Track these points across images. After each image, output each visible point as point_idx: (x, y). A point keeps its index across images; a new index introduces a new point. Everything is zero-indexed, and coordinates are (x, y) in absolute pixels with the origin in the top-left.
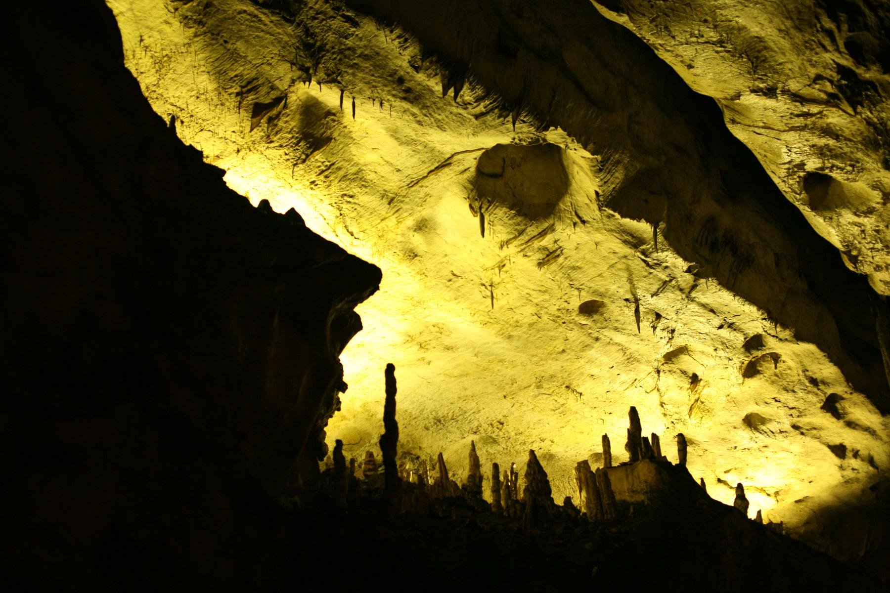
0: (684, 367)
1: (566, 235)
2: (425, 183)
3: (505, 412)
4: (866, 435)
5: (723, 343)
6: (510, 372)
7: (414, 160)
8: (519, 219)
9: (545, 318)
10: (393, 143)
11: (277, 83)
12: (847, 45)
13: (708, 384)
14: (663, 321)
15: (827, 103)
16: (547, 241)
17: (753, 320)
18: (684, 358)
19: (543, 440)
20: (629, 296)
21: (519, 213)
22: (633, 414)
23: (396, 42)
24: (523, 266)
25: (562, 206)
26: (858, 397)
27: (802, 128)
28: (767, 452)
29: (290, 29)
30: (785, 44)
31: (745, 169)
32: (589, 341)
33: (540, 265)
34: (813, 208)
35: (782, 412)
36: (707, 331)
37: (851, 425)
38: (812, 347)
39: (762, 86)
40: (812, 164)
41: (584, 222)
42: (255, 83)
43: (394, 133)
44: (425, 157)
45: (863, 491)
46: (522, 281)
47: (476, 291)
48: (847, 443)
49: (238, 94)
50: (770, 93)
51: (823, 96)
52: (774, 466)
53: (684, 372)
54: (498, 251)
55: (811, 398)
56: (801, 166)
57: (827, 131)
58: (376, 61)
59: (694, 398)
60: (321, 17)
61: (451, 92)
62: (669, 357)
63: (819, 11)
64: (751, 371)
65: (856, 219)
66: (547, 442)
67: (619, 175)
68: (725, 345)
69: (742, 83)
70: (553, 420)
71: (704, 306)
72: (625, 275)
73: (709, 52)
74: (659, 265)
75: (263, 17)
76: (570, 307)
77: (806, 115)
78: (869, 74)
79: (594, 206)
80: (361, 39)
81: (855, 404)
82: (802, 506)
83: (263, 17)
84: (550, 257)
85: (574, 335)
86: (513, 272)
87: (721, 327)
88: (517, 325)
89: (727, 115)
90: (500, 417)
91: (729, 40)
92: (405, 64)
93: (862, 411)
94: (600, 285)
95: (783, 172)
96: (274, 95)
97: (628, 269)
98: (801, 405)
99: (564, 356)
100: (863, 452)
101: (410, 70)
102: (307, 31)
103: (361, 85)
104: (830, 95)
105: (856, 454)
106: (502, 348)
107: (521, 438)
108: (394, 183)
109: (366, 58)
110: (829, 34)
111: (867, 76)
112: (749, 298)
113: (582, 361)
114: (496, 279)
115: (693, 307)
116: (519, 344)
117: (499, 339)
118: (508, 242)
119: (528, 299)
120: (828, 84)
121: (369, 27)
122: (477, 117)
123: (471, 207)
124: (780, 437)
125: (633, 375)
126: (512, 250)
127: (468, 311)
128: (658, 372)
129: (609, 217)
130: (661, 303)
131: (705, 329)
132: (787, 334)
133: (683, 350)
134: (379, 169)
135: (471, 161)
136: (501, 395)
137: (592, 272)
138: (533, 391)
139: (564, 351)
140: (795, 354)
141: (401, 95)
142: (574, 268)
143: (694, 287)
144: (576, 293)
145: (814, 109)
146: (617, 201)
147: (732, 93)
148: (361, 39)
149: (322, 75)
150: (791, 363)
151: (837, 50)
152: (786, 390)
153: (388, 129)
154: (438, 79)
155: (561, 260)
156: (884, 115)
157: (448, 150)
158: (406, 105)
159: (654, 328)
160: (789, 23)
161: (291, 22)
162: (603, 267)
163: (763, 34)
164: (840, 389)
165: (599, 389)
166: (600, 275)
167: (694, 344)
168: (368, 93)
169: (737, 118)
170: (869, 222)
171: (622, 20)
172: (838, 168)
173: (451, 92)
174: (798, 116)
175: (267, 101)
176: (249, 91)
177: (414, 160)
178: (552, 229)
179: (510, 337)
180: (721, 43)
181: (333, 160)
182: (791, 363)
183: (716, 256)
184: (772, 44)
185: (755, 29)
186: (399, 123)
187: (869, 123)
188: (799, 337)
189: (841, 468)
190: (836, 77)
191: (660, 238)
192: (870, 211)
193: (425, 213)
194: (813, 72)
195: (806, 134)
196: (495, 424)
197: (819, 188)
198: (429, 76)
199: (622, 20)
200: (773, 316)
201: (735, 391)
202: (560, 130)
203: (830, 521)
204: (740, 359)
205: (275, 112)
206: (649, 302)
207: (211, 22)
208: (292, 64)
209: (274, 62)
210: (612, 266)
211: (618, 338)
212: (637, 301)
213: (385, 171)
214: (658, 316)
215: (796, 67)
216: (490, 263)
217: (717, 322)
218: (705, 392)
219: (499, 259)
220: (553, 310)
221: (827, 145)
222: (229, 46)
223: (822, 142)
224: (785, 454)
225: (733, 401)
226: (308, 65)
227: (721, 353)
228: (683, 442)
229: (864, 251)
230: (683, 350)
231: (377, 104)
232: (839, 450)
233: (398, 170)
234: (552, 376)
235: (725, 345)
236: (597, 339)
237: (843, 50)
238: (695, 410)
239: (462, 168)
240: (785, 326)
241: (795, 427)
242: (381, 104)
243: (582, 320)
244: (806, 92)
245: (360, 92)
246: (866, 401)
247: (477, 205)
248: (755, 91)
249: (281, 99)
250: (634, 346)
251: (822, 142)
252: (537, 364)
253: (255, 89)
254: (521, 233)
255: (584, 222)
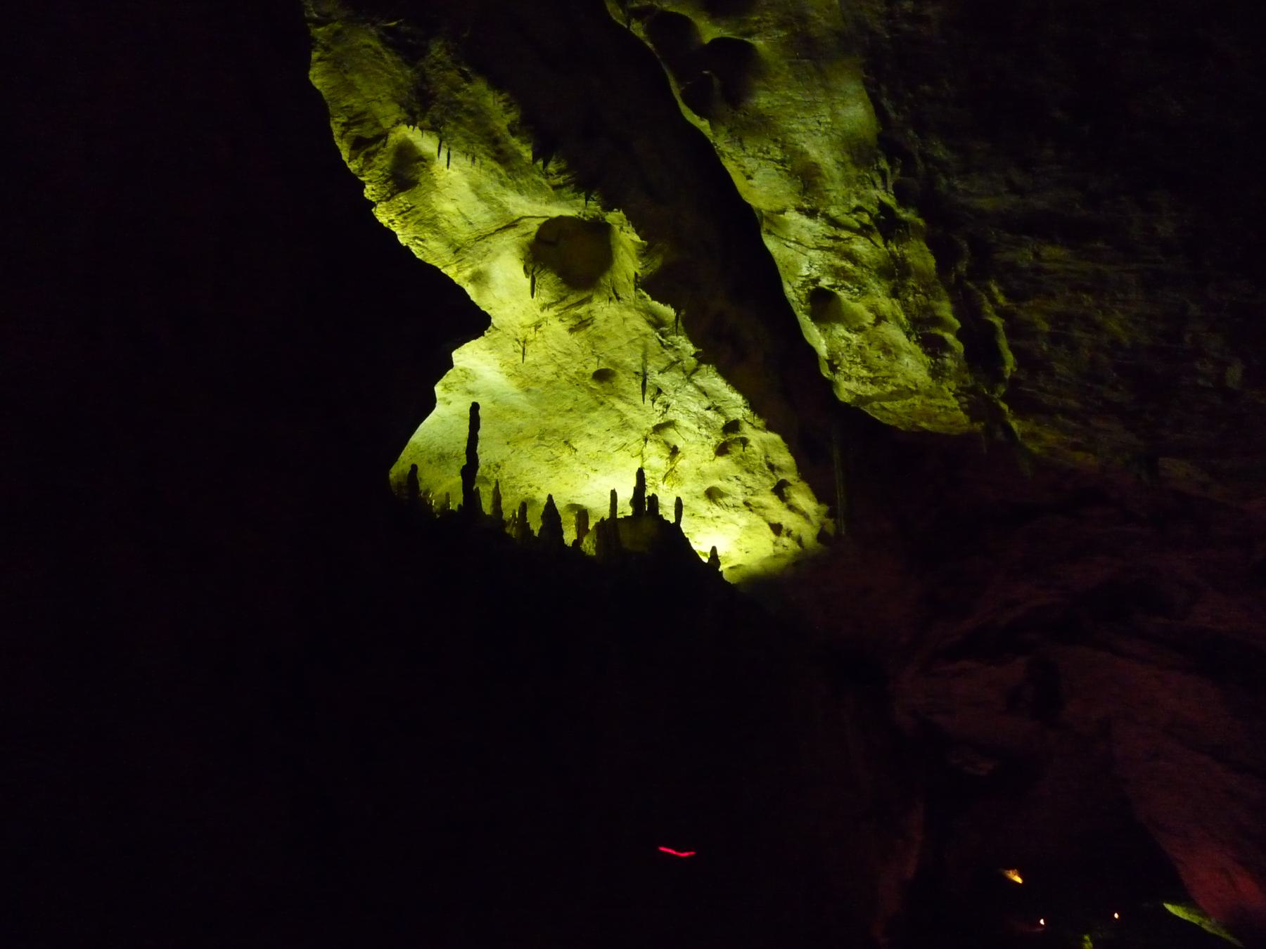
0: (668, 439)
1: (602, 309)
2: (491, 239)
3: (505, 457)
4: (801, 518)
5: (707, 423)
6: (518, 422)
7: (487, 217)
8: (564, 286)
9: (563, 377)
10: (472, 197)
11: (382, 121)
12: (895, 187)
13: (684, 457)
14: (663, 396)
15: (859, 232)
16: (582, 311)
17: (736, 405)
18: (671, 431)
19: (530, 486)
20: (639, 370)
21: (564, 281)
22: (640, 474)
23: (501, 105)
24: (557, 328)
25: (602, 281)
26: (803, 486)
27: (829, 249)
28: (719, 522)
29: (408, 72)
30: (837, 174)
31: (766, 272)
32: (594, 404)
33: (571, 330)
34: (814, 319)
35: (739, 490)
36: (695, 410)
37: (791, 508)
38: (777, 437)
39: (806, 206)
40: (825, 282)
41: (618, 298)
42: (363, 118)
43: (476, 189)
44: (496, 215)
45: (787, 566)
46: (551, 342)
47: (510, 345)
48: (784, 523)
49: (344, 124)
50: (811, 214)
51: (857, 225)
52: (733, 538)
53: (667, 443)
54: (538, 312)
55: (767, 481)
56: (816, 281)
57: (850, 256)
58: (478, 116)
59: (669, 467)
60: (440, 66)
61: (540, 163)
62: (658, 429)
63: (879, 152)
64: (722, 450)
65: (847, 334)
66: (534, 489)
67: (658, 262)
68: (708, 424)
69: (790, 202)
70: (545, 469)
71: (700, 388)
72: (640, 351)
73: (771, 168)
74: (670, 346)
75: (386, 56)
76: (587, 372)
77: (836, 238)
78: (906, 215)
79: (632, 286)
80: (470, 95)
81: (799, 491)
82: (734, 572)
83: (386, 56)
84: (581, 324)
85: (584, 397)
86: (546, 333)
87: (709, 409)
88: (538, 380)
89: (765, 225)
90: (498, 460)
91: (791, 161)
92: (504, 127)
93: (804, 499)
94: (617, 356)
95: (798, 283)
96: (377, 131)
97: (645, 346)
98: (756, 486)
99: (572, 415)
100: (795, 533)
101: (507, 133)
102: (424, 79)
103: (459, 138)
104: (864, 226)
105: (789, 534)
106: (520, 400)
107: (512, 482)
108: (464, 234)
109: (470, 113)
110: (883, 174)
111: (904, 216)
112: (738, 387)
113: (585, 421)
114: (530, 337)
115: (690, 388)
116: (534, 397)
117: (516, 391)
118: (549, 306)
119: (553, 359)
120: (867, 216)
121: (480, 86)
122: (555, 187)
123: (525, 268)
124: (732, 511)
125: (624, 440)
126: (550, 313)
127: (498, 362)
128: (646, 440)
129: (642, 297)
130: (664, 380)
131: (695, 408)
132: (760, 423)
133: (671, 424)
134: (452, 219)
135: (533, 226)
136: (504, 441)
137: (613, 344)
138: (535, 441)
139: (571, 410)
140: (760, 439)
141: (493, 154)
142: (601, 338)
143: (695, 371)
144: (596, 360)
145: (845, 234)
146: (651, 285)
147: (779, 207)
148: (470, 95)
149: (426, 122)
150: (756, 448)
151: (886, 189)
152: (748, 471)
153: (471, 184)
154: (529, 147)
155: (590, 328)
156: (906, 252)
157: (518, 212)
158: (495, 165)
159: (654, 401)
160: (847, 158)
161: (411, 65)
162: (624, 341)
163: (820, 161)
164: (791, 477)
165: (593, 447)
166: (620, 348)
167: (683, 421)
168: (464, 147)
169: (773, 230)
170: (855, 339)
171: (703, 125)
172: (847, 288)
173: (540, 163)
174: (829, 238)
175: (369, 136)
176: (355, 124)
177: (487, 217)
178: (589, 300)
179: (528, 391)
180: (782, 162)
181: (414, 203)
182: (756, 448)
183: (721, 348)
184: (825, 172)
185: (814, 153)
186: (483, 180)
187: (892, 255)
188: (769, 427)
189: (775, 544)
190: (876, 211)
191: (680, 324)
192: (860, 330)
193: (482, 266)
194: (855, 202)
195: (831, 255)
196: (493, 466)
197: (823, 304)
198: (522, 142)
199: (703, 125)
200: (755, 405)
201: (705, 466)
202: (621, 213)
203: (761, 586)
204: (717, 438)
205: (373, 148)
206: (656, 378)
207: (338, 49)
208: (402, 105)
209: (384, 99)
210: (632, 341)
211: (620, 405)
212: (645, 376)
213: (458, 222)
214: (659, 391)
215: (840, 197)
216: (528, 322)
217: (706, 403)
218: (681, 463)
219: (536, 319)
220: (572, 372)
221: (843, 267)
222: (348, 77)
223: (838, 262)
224: (734, 526)
225: (701, 475)
226: (417, 109)
227: (704, 432)
228: (679, 505)
229: (844, 361)
230: (671, 424)
231: (470, 159)
232: (777, 528)
233: (470, 223)
234: (555, 431)
235: (708, 424)
236: (602, 403)
237: (890, 190)
238: (669, 478)
239: (525, 231)
240: (761, 416)
241: (746, 504)
242: (473, 160)
243: (594, 385)
244: (844, 219)
245: (457, 145)
246: (809, 490)
247: (530, 267)
248: (800, 210)
249: (383, 136)
250: (632, 415)
251: (838, 262)
252: (544, 417)
253: (360, 123)
254: (563, 299)
255: (618, 298)
